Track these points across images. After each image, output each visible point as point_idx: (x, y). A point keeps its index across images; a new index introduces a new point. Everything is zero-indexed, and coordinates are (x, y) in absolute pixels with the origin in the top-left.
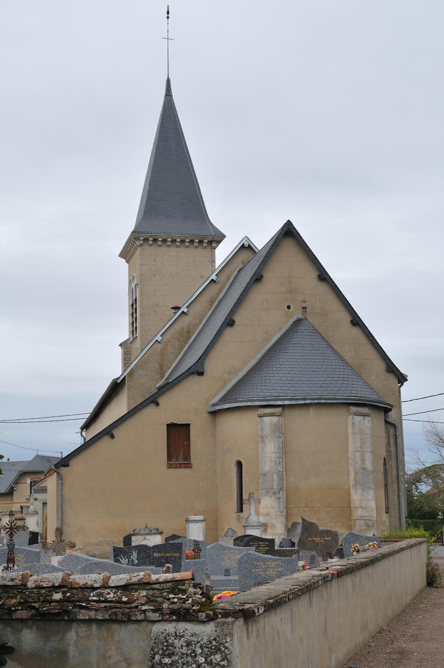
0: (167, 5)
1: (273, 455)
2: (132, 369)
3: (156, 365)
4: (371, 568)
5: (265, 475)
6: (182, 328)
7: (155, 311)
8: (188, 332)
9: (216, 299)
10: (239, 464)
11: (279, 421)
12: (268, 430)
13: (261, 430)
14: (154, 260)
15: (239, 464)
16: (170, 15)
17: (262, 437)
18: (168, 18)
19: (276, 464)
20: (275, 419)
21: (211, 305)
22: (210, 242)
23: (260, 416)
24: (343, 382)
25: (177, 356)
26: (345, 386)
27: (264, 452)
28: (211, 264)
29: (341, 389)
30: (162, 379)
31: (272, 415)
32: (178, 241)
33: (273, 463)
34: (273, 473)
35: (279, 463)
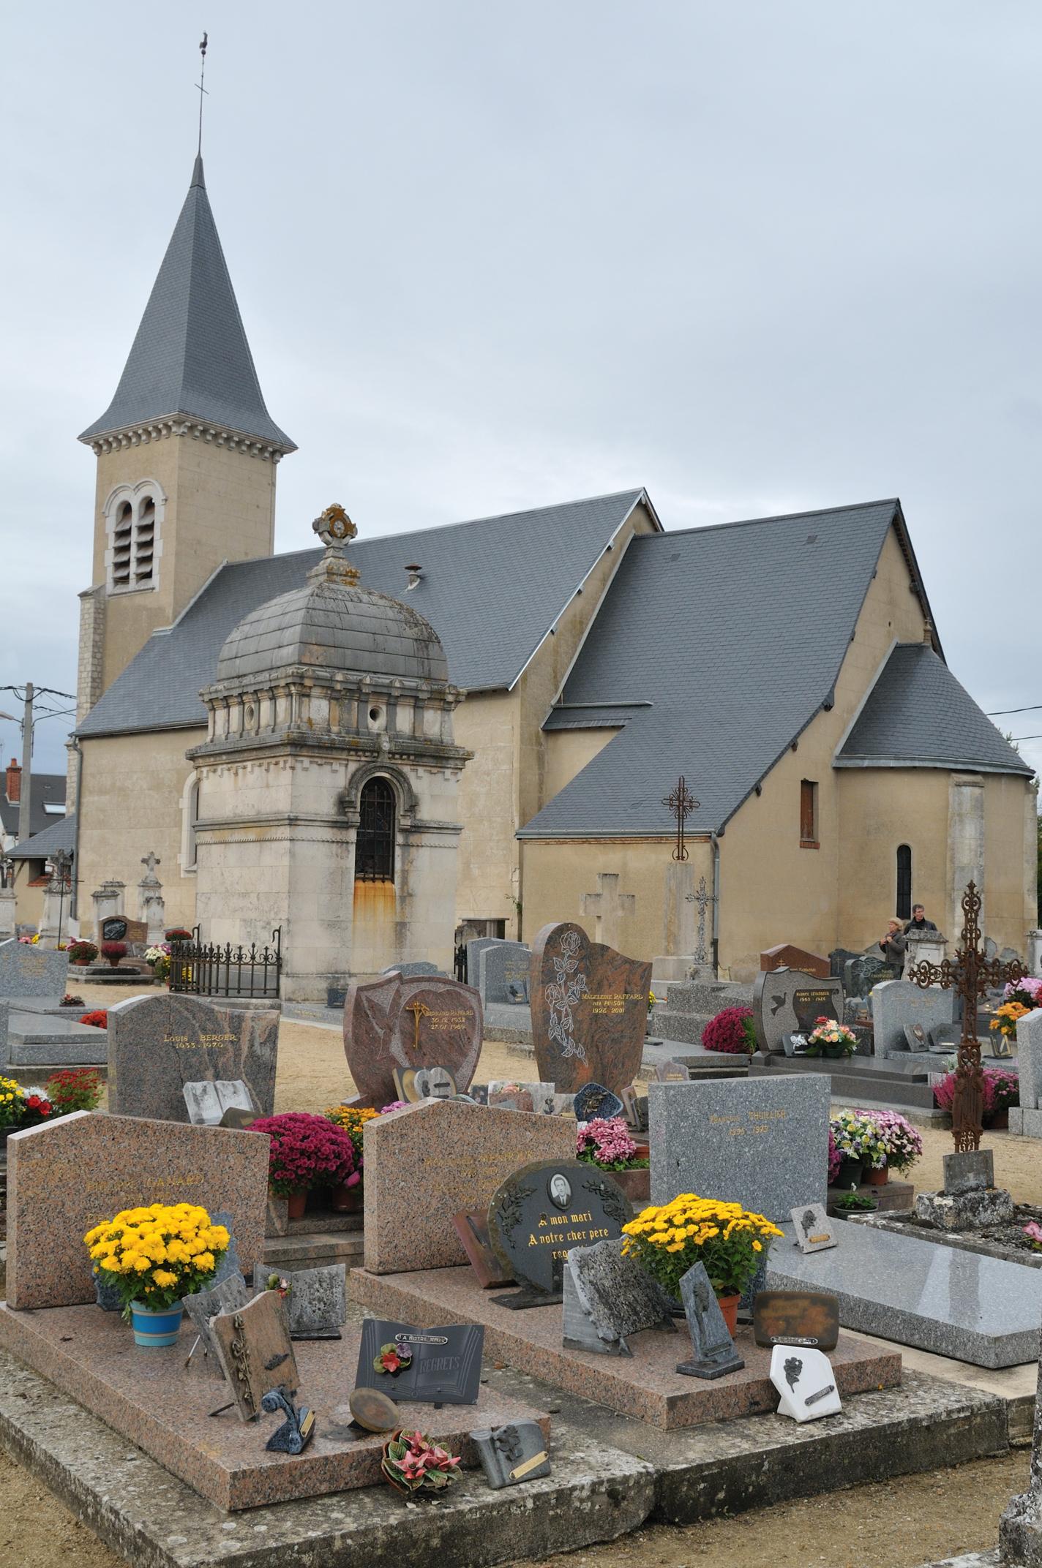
0: (202, 32)
1: (973, 842)
2: (525, 672)
3: (550, 669)
4: (408, 933)
5: (962, 869)
6: (575, 616)
7: (195, 552)
8: (581, 623)
9: (609, 576)
10: (904, 852)
11: (981, 794)
12: (967, 806)
13: (959, 804)
14: (199, 465)
15: (904, 852)
16: (207, 49)
17: (960, 815)
18: (204, 53)
19: (976, 855)
20: (977, 791)
21: (604, 585)
22: (273, 453)
23: (958, 785)
24: (968, 738)
25: (572, 658)
26: (971, 739)
27: (962, 837)
28: (269, 487)
29: (963, 746)
30: (556, 692)
31: (974, 785)
32: (234, 441)
33: (973, 853)
34: (973, 867)
35: (981, 854)
